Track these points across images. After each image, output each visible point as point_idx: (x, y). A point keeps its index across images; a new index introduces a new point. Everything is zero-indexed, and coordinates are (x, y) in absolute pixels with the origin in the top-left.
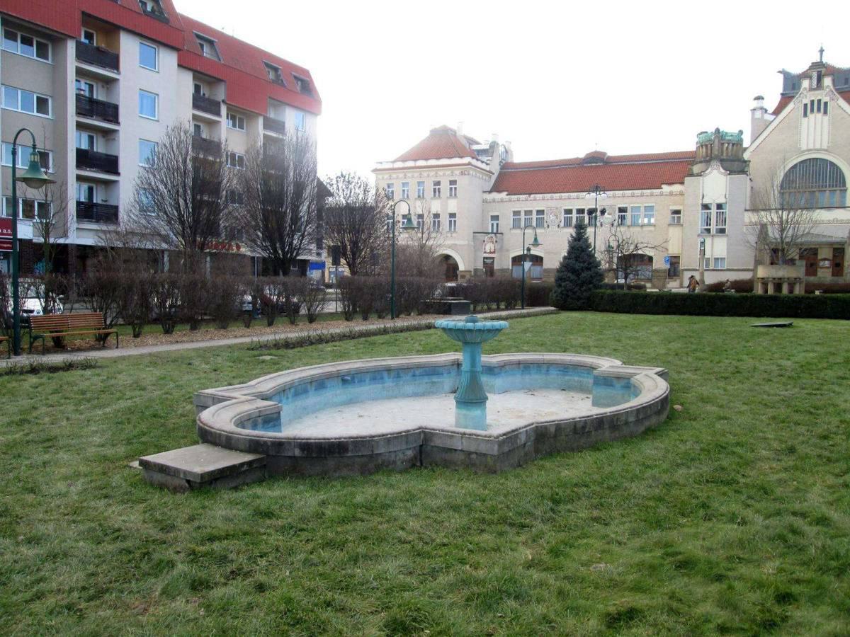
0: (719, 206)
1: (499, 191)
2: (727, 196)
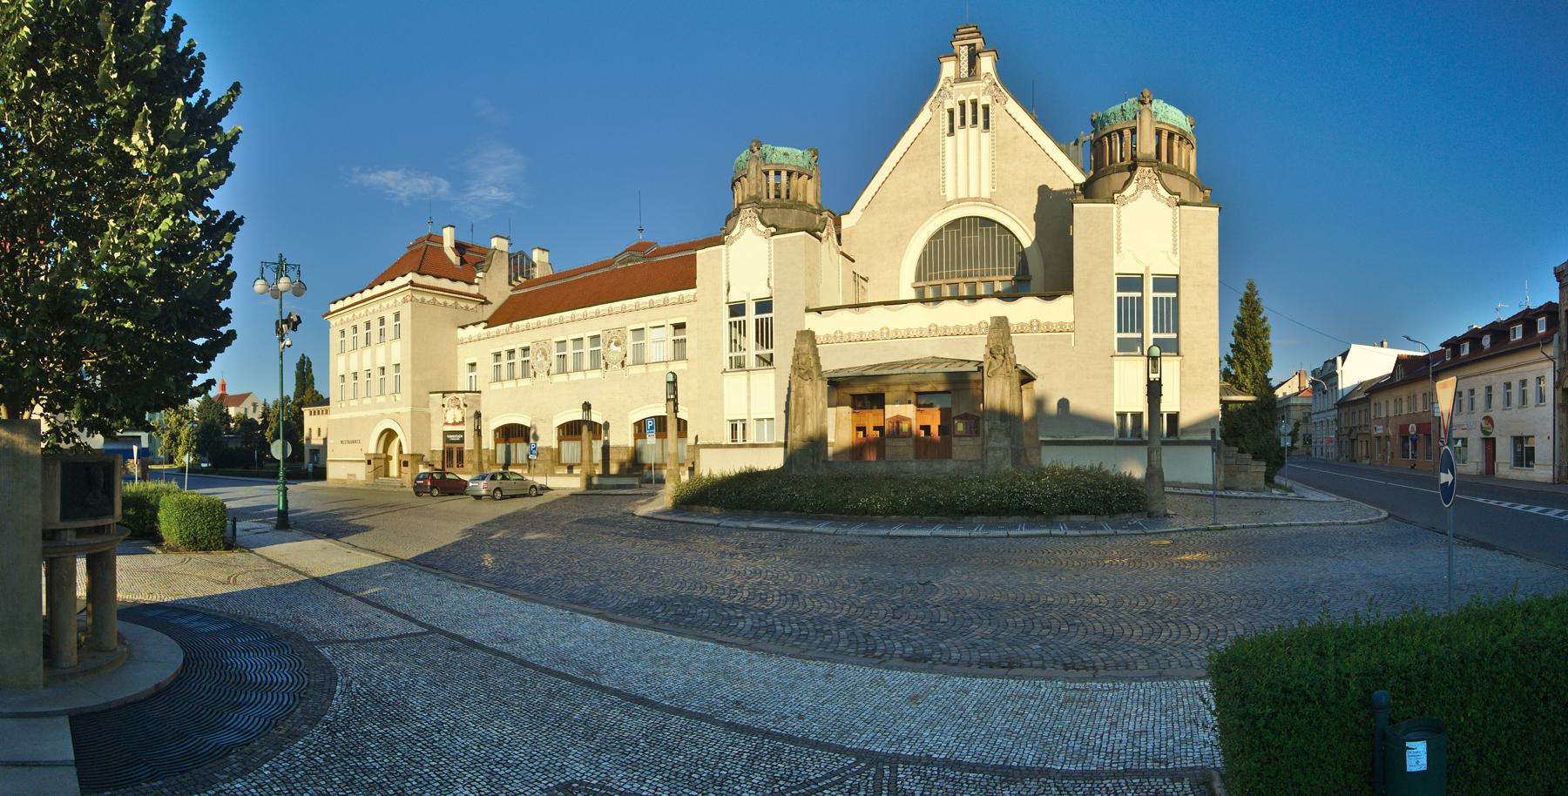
2: (772, 284)
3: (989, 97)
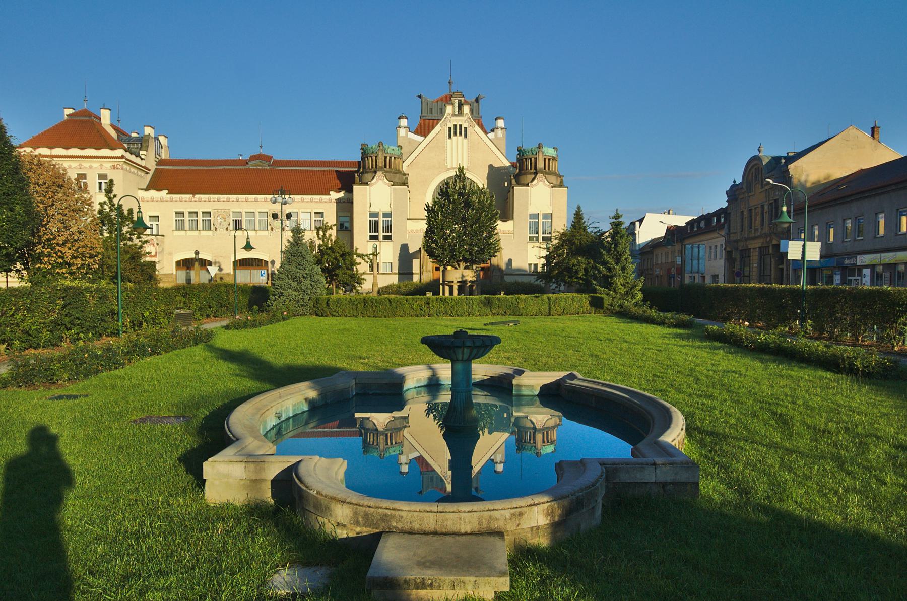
0: (546, 216)
1: (159, 190)
2: (392, 206)
3: (467, 124)
